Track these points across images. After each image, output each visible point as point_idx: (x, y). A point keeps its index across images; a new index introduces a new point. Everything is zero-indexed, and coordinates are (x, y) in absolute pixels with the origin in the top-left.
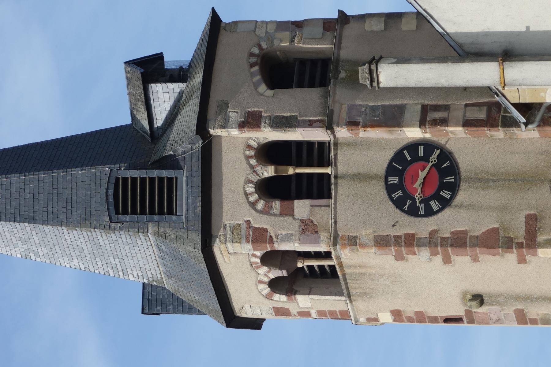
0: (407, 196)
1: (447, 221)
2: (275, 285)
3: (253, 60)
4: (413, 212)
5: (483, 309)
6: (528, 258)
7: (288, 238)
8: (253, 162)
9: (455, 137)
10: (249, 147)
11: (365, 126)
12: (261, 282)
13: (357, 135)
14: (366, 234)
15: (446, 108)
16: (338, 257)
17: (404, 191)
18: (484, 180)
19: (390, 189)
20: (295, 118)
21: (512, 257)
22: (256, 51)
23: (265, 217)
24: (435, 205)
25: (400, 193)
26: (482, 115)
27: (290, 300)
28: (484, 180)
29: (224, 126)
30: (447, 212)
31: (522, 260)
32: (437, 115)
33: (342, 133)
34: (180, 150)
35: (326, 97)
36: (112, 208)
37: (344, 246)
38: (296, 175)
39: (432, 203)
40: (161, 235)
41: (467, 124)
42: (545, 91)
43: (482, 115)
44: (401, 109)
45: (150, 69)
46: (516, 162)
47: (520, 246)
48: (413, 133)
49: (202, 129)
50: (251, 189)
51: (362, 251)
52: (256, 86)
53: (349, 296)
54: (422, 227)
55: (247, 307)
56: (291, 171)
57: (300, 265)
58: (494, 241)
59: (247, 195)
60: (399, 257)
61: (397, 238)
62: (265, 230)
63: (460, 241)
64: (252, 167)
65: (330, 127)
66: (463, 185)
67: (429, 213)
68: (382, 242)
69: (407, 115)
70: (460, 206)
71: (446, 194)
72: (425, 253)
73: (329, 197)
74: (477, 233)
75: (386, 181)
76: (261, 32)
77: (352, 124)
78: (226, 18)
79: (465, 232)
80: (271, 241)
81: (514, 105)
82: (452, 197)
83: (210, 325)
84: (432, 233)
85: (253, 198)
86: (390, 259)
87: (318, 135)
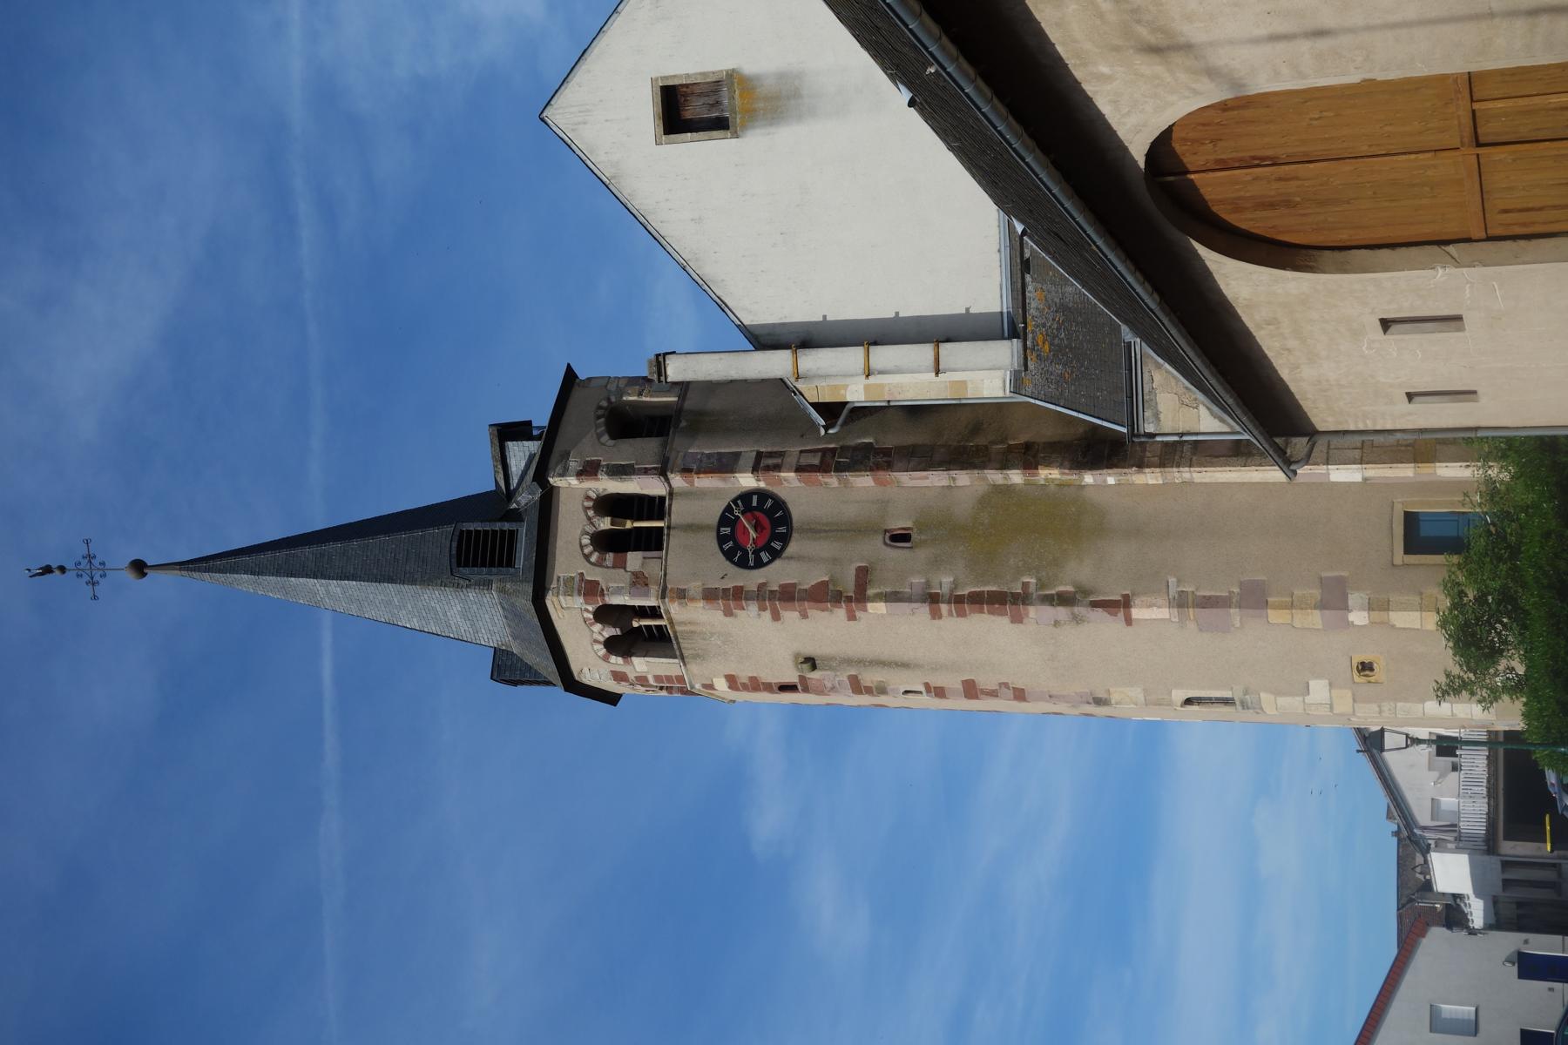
0: (738, 547)
1: (777, 574)
2: (612, 645)
3: (600, 412)
4: (743, 564)
5: (815, 675)
6: (858, 614)
7: (618, 591)
8: (591, 513)
9: (788, 484)
10: (588, 498)
11: (698, 472)
12: (596, 641)
13: (692, 483)
14: (695, 587)
15: (781, 454)
16: (668, 612)
17: (735, 542)
18: (817, 530)
19: (722, 540)
20: (632, 466)
21: (841, 612)
22: (604, 404)
23: (598, 569)
24: (765, 556)
25: (731, 544)
26: (816, 461)
27: (626, 662)
28: (817, 530)
29: (562, 475)
30: (777, 563)
31: (852, 617)
32: (770, 462)
33: (677, 481)
34: (523, 502)
35: (664, 446)
36: (454, 560)
37: (672, 600)
38: (631, 528)
39: (762, 554)
40: (502, 591)
41: (799, 469)
42: (846, 387)
43: (816, 461)
44: (737, 455)
45: (509, 432)
46: (850, 512)
47: (849, 599)
48: (747, 481)
49: (541, 477)
50: (586, 540)
51: (691, 605)
52: (599, 436)
53: (683, 658)
54: (752, 579)
55: (586, 670)
56: (629, 525)
57: (635, 624)
58: (825, 595)
59: (582, 547)
60: (728, 613)
61: (725, 590)
62: (597, 583)
63: (788, 595)
64: (589, 519)
65: (663, 472)
66: (795, 535)
67: (759, 564)
68: (710, 595)
69: (741, 462)
70: (790, 558)
71: (777, 545)
72: (753, 607)
73: (660, 549)
74: (806, 587)
75: (718, 531)
76: (612, 387)
77: (686, 471)
78: (582, 374)
79: (794, 585)
80: (602, 594)
81: (812, 404)
82: (783, 548)
83: (558, 691)
84: (761, 586)
85: (586, 551)
86: (720, 614)
87: (651, 486)
